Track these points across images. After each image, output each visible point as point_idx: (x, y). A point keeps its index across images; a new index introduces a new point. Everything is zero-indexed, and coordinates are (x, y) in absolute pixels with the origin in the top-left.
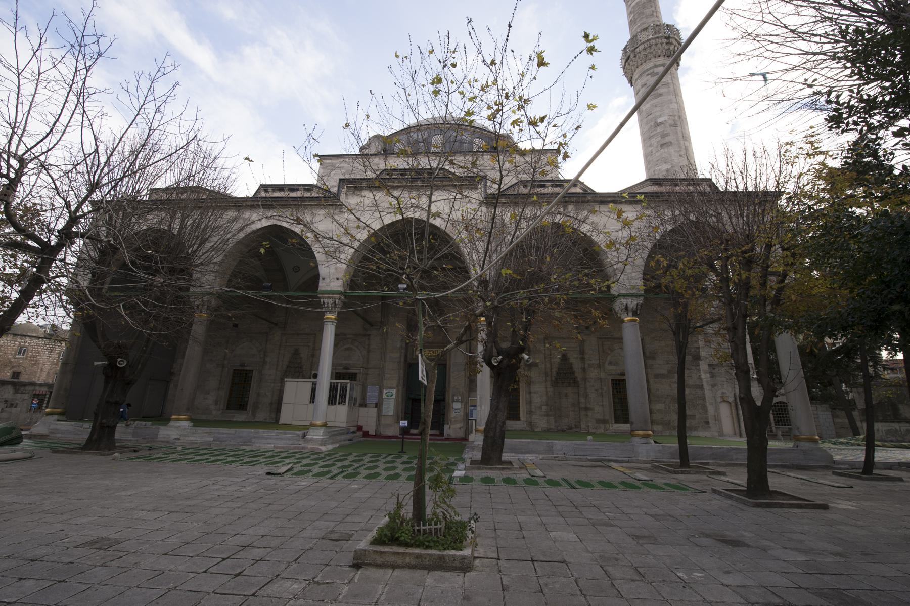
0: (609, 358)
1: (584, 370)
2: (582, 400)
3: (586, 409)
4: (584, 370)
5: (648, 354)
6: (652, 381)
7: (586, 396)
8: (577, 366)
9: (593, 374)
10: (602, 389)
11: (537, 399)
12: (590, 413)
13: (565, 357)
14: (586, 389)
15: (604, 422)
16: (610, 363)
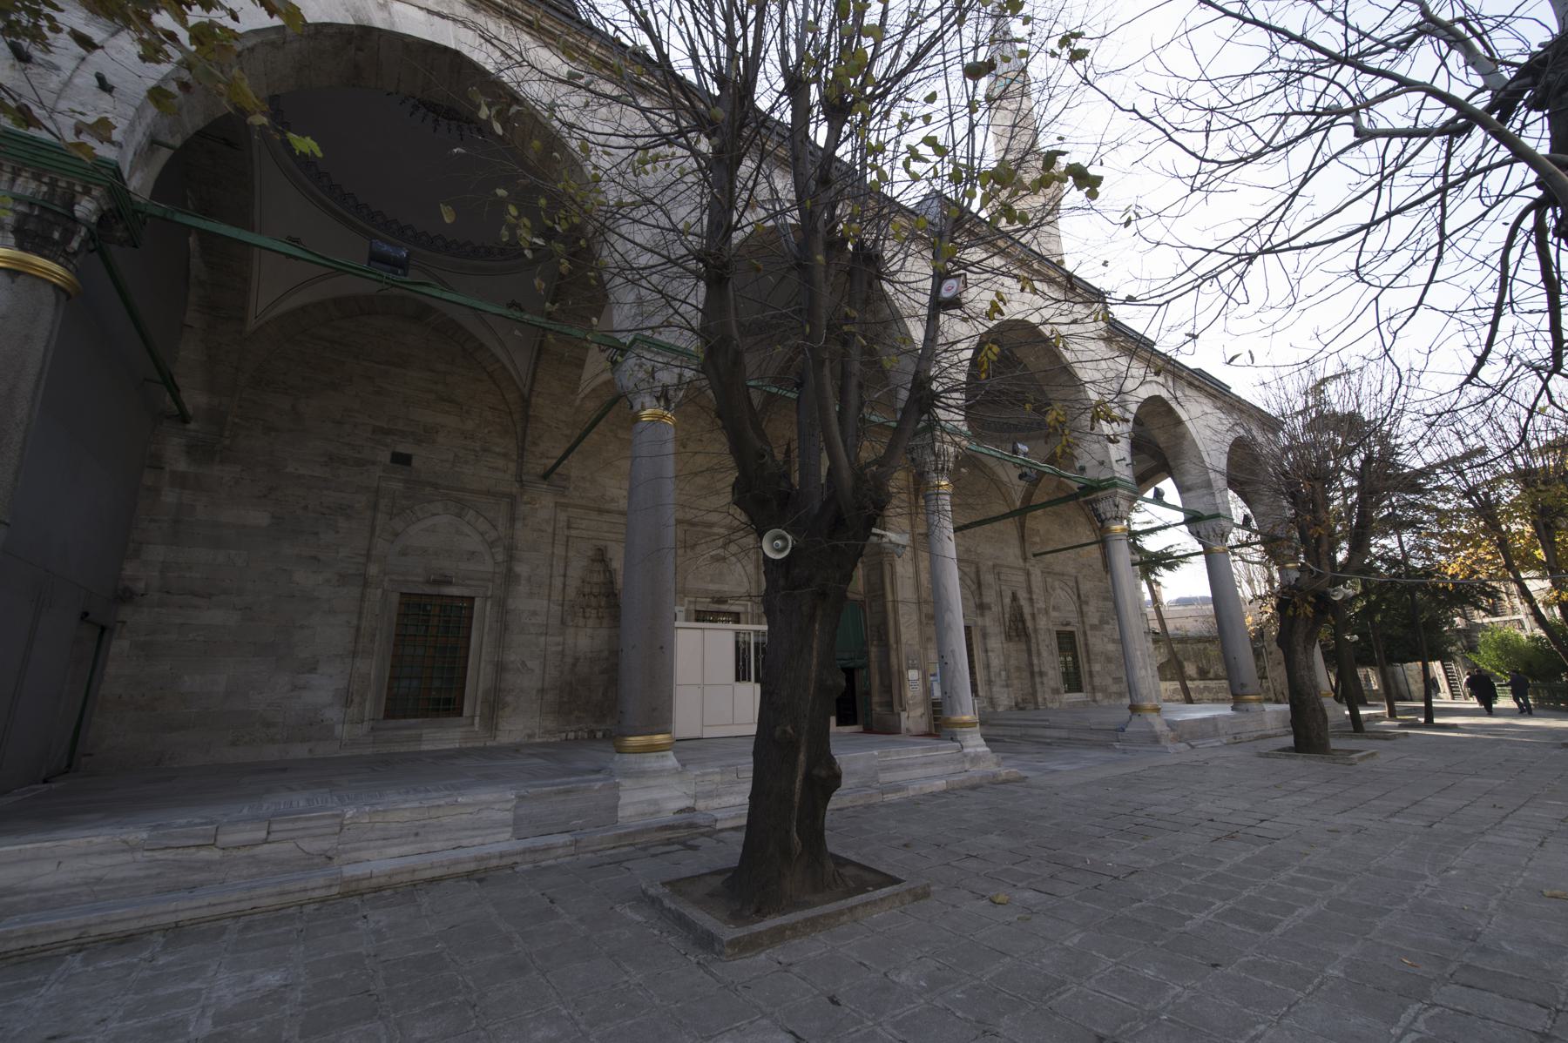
1: (1033, 616)
2: (1035, 661)
3: (1041, 674)
4: (1033, 616)
7: (1039, 654)
8: (1027, 610)
9: (1042, 622)
11: (996, 662)
12: (1045, 680)
13: (1014, 598)
15: (1056, 691)
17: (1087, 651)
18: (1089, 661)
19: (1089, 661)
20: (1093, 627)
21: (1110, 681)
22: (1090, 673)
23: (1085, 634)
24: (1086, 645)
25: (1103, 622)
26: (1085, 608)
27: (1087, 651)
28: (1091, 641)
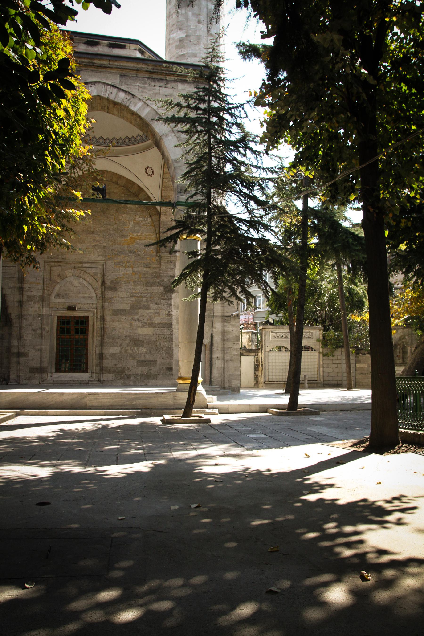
0: (57, 288)
3: (19, 354)
4: (21, 303)
5: (108, 284)
6: (108, 318)
9: (32, 309)
10: (42, 329)
12: (23, 360)
14: (21, 329)
16: (58, 295)
17: (102, 337)
18: (102, 343)
19: (102, 343)
20: (116, 312)
21: (132, 363)
22: (101, 356)
23: (103, 319)
24: (103, 329)
25: (134, 307)
26: (109, 294)
27: (102, 337)
28: (110, 323)
